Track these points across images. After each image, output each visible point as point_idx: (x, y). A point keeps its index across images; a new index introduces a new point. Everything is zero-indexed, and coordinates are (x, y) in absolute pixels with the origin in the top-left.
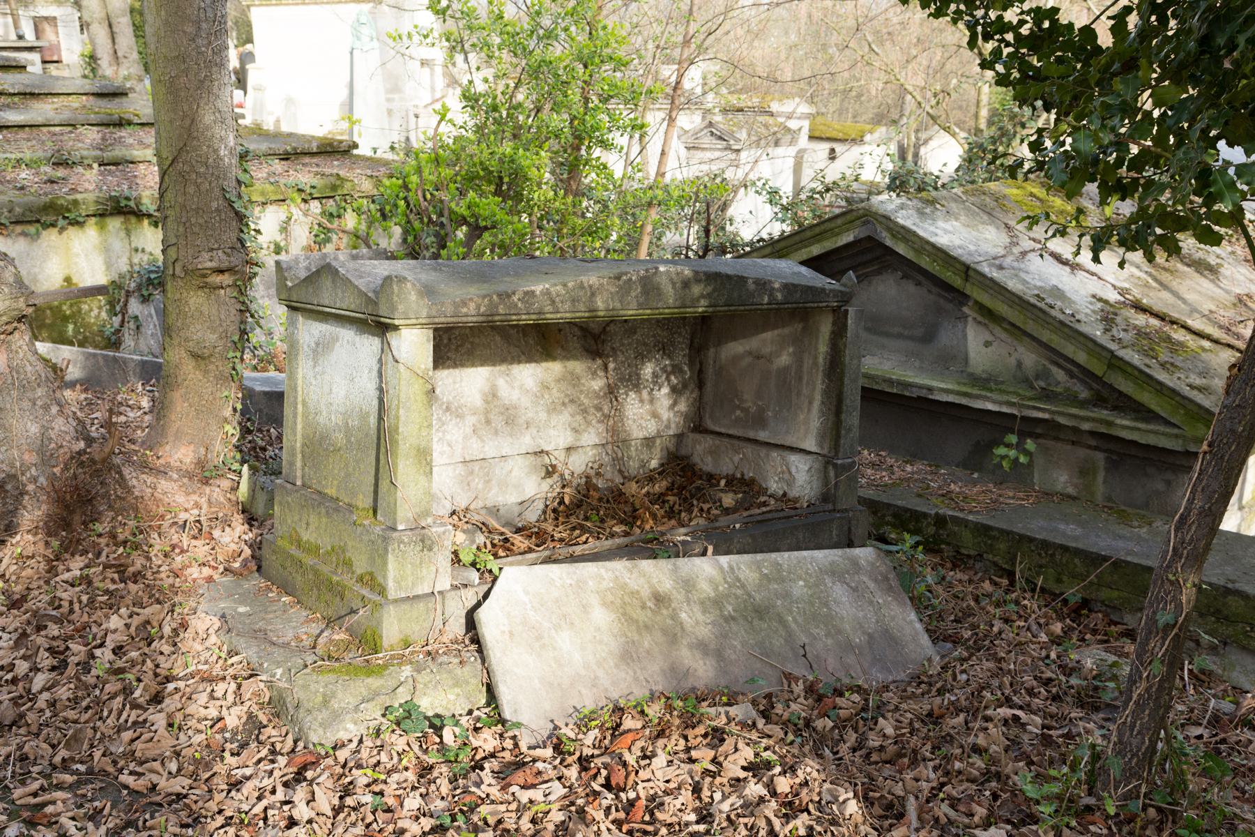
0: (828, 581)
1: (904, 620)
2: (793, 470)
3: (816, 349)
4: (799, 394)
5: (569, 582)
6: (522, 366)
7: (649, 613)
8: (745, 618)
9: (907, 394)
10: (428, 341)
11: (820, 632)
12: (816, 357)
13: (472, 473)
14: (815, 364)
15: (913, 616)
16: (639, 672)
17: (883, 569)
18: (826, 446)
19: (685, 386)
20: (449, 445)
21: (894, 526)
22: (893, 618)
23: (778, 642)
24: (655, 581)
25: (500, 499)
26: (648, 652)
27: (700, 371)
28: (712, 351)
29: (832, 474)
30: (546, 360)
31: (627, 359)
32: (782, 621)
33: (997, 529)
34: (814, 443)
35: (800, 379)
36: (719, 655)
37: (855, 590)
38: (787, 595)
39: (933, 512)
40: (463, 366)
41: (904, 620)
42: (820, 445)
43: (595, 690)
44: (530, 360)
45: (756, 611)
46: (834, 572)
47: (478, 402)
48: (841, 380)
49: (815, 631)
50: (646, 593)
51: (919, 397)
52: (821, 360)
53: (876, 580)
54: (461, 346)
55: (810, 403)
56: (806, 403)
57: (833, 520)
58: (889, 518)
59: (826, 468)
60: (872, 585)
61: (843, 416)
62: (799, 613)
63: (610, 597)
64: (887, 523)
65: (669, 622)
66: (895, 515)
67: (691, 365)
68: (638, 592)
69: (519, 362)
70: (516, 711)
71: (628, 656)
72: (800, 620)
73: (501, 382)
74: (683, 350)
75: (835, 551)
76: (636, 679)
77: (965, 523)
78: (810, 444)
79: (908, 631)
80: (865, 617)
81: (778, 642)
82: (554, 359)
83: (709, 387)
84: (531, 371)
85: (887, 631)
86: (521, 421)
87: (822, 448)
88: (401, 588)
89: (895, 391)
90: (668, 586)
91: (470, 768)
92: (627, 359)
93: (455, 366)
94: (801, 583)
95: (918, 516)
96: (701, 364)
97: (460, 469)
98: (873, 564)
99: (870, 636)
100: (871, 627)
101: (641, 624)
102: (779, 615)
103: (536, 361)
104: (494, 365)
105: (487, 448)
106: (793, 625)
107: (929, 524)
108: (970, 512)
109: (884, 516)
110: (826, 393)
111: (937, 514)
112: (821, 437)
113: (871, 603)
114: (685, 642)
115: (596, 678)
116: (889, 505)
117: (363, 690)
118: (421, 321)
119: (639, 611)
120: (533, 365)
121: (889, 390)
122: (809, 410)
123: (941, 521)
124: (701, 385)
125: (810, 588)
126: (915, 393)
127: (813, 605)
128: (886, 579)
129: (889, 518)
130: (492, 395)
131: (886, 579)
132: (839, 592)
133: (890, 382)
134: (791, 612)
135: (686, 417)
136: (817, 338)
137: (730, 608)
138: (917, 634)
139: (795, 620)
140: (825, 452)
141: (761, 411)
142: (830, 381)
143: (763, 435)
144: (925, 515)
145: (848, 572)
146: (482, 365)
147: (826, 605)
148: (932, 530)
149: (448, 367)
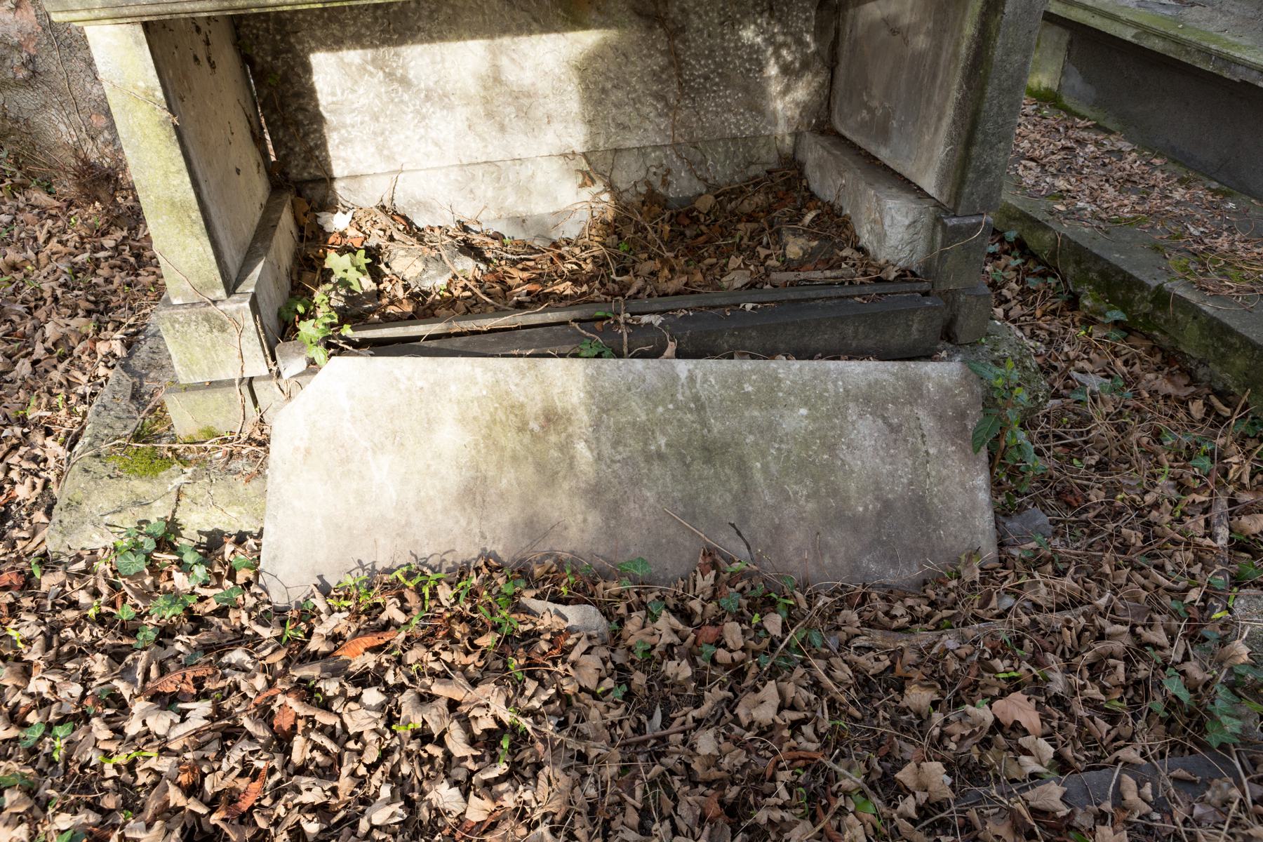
0: (853, 411)
1: (962, 485)
2: (887, 221)
3: (961, 30)
4: (929, 102)
5: (420, 384)
6: (535, 38)
7: (527, 439)
8: (682, 458)
9: (1227, 75)
10: (137, 43)
11: (799, 489)
12: (958, 44)
13: (473, 178)
14: (956, 55)
15: (981, 480)
16: (476, 521)
17: (963, 399)
18: (946, 191)
19: (805, 65)
20: (436, 144)
21: (1098, 288)
22: (941, 481)
23: (720, 500)
24: (556, 391)
25: (521, 209)
26: (501, 495)
27: (835, 45)
28: (851, 11)
29: (939, 238)
30: (574, 30)
31: (706, 25)
32: (742, 468)
33: (1241, 336)
34: (933, 183)
35: (935, 76)
36: (613, 511)
37: (894, 429)
38: (768, 430)
39: (1154, 284)
40: (442, 38)
41: (962, 485)
42: (940, 187)
43: (399, 541)
44: (547, 28)
45: (706, 449)
46: (871, 400)
47: (473, 88)
48: (982, 89)
49: (791, 488)
50: (534, 408)
51: (1244, 83)
52: (963, 50)
53: (941, 418)
54: (437, 10)
55: (940, 119)
56: (934, 119)
57: (914, 311)
58: (1093, 275)
59: (935, 226)
60: (928, 423)
61: (975, 151)
62: (777, 458)
63: (475, 410)
64: (1091, 282)
65: (555, 453)
66: (1102, 274)
67: (819, 34)
68: (522, 406)
69: (531, 32)
70: (274, 558)
71: (474, 494)
72: (774, 468)
73: (504, 61)
74: (805, 10)
75: (889, 364)
76: (467, 532)
77: (1195, 312)
78: (929, 183)
79: (960, 502)
80: (891, 474)
81: (720, 500)
82: (586, 27)
83: (841, 71)
84: (550, 45)
85: (921, 499)
86: (540, 112)
87: (941, 194)
88: (193, 373)
89: (1210, 68)
90: (575, 400)
91: (194, 618)
92: (706, 25)
93: (431, 39)
94: (803, 411)
95: (1133, 284)
96: (837, 32)
97: (455, 174)
98: (948, 390)
99: (887, 505)
100: (896, 491)
101: (508, 453)
102: (741, 458)
103: (556, 31)
104: (492, 37)
105: (490, 149)
106: (758, 476)
107: (1143, 299)
108: (1216, 295)
109: (1089, 269)
110: (960, 106)
111: (1159, 288)
112: (944, 176)
113: (914, 452)
114: (566, 486)
115: (408, 524)
116: (1098, 258)
117: (123, 494)
118: (96, 13)
119: (512, 434)
120: (553, 36)
121: (1203, 67)
122: (937, 130)
123: (1161, 298)
124: (832, 68)
125: (815, 420)
126: (1238, 75)
127: (808, 447)
128: (962, 415)
129: (1093, 275)
130: (496, 78)
131: (962, 415)
132: (865, 431)
133: (1207, 53)
134: (763, 454)
135: (805, 108)
136: (965, 9)
137: (662, 441)
138: (974, 507)
139: (765, 469)
140: (943, 200)
141: (888, 116)
142: (969, 88)
143: (883, 154)
144: (1142, 286)
145: (895, 401)
146: (473, 38)
147: (832, 448)
148: (1146, 307)
149: (421, 42)
